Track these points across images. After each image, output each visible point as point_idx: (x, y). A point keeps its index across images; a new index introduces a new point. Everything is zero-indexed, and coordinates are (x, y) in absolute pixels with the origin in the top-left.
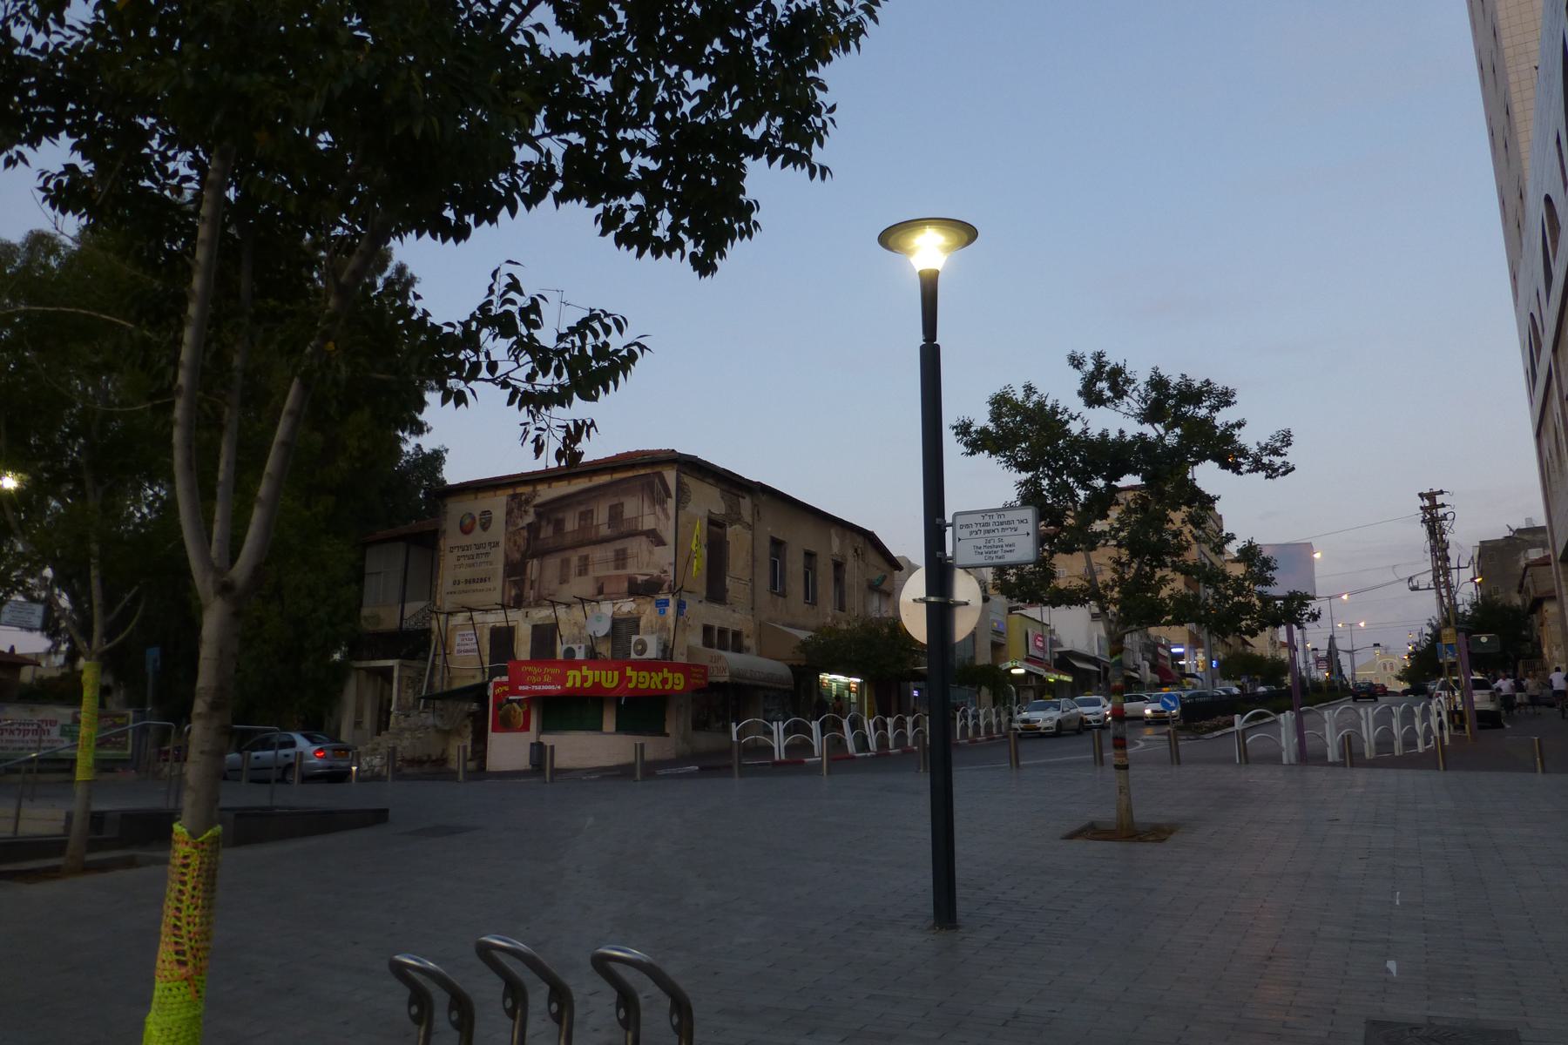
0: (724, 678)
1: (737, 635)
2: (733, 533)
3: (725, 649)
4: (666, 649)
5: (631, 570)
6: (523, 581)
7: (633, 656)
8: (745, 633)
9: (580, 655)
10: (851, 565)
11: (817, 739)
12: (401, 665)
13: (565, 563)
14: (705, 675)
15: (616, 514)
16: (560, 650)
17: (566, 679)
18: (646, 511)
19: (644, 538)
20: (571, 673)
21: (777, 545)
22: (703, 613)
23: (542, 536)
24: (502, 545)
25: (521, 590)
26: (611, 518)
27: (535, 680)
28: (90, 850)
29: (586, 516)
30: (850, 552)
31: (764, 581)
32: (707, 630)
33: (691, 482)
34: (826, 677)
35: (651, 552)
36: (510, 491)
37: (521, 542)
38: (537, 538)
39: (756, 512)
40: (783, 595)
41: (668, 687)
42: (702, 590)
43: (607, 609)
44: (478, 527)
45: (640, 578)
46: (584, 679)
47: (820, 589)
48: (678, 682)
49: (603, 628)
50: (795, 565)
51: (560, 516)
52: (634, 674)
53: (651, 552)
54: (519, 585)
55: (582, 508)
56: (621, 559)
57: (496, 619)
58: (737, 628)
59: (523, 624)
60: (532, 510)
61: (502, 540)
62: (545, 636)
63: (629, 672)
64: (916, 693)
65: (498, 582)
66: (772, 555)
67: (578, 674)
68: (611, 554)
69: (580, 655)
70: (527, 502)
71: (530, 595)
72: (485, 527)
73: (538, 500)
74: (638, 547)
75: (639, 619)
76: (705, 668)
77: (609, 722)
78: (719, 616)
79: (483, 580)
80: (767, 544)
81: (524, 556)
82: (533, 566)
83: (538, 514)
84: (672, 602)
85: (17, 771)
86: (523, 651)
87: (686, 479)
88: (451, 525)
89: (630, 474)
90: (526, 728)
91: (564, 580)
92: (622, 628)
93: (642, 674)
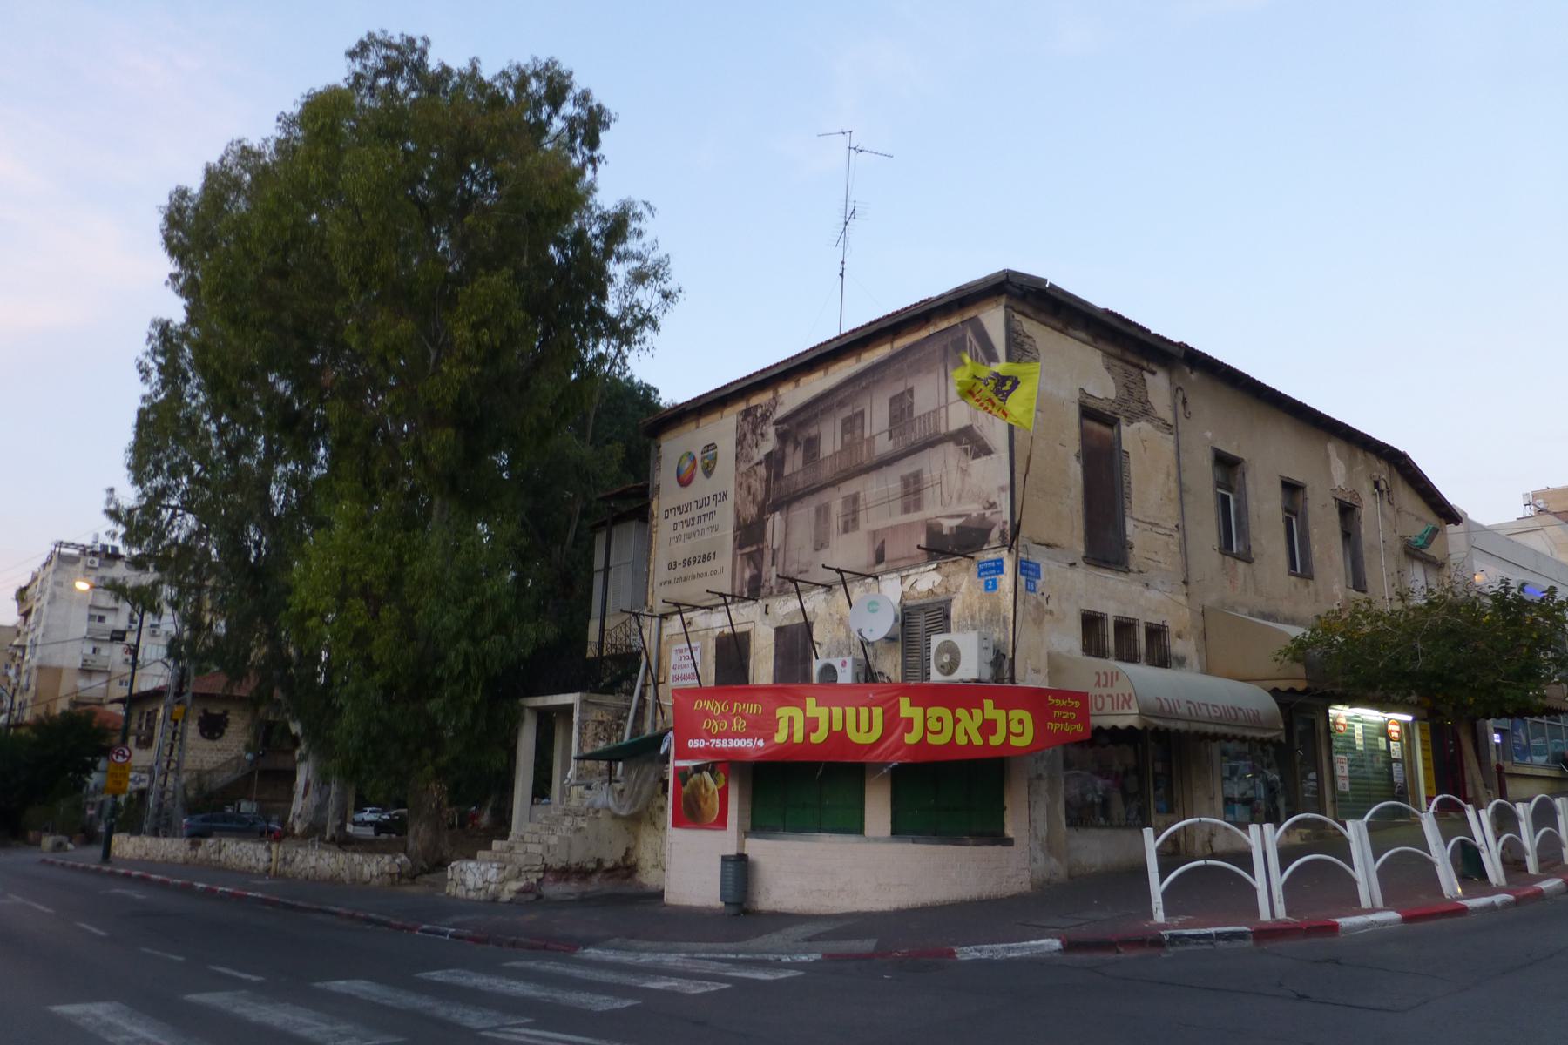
0: (1128, 718)
1: (1156, 633)
2: (1133, 435)
3: (1133, 659)
4: (1000, 660)
6: (761, 552)
7: (936, 677)
8: (1173, 627)
9: (845, 676)
10: (1371, 512)
11: (1364, 868)
12: (583, 701)
13: (823, 512)
14: (1083, 714)
15: (901, 410)
16: (816, 666)
17: (774, 726)
20: (783, 712)
21: (1227, 464)
22: (1078, 588)
23: (787, 471)
24: (731, 496)
25: (758, 567)
27: (716, 727)
29: (853, 423)
30: (1366, 489)
31: (1206, 532)
32: (1091, 622)
33: (1036, 331)
34: (1340, 713)
35: (964, 472)
36: (742, 406)
37: (758, 487)
38: (779, 476)
39: (1181, 401)
40: (1247, 559)
41: (996, 740)
42: (1074, 537)
43: (891, 589)
44: (699, 472)
45: (948, 525)
46: (811, 725)
47: (1316, 550)
48: (1018, 728)
49: (880, 625)
50: (1265, 504)
51: (813, 431)
52: (916, 714)
53: (964, 472)
54: (755, 559)
55: (847, 412)
56: (913, 491)
57: (717, 622)
58: (1156, 619)
59: (760, 624)
60: (770, 431)
61: (731, 489)
62: (795, 644)
63: (906, 708)
64: (1497, 738)
65: (725, 559)
66: (1218, 485)
67: (796, 712)
69: (845, 676)
70: (765, 418)
71: (771, 574)
72: (708, 472)
73: (780, 412)
74: (941, 465)
75: (949, 602)
76: (1083, 697)
77: (878, 810)
78: (1114, 596)
79: (706, 558)
80: (1207, 461)
81: (762, 510)
82: (775, 524)
83: (782, 437)
84: (1009, 566)
86: (762, 670)
87: (1029, 326)
88: (665, 476)
89: (923, 334)
90: (721, 822)
91: (821, 544)
92: (919, 623)
93: (935, 712)
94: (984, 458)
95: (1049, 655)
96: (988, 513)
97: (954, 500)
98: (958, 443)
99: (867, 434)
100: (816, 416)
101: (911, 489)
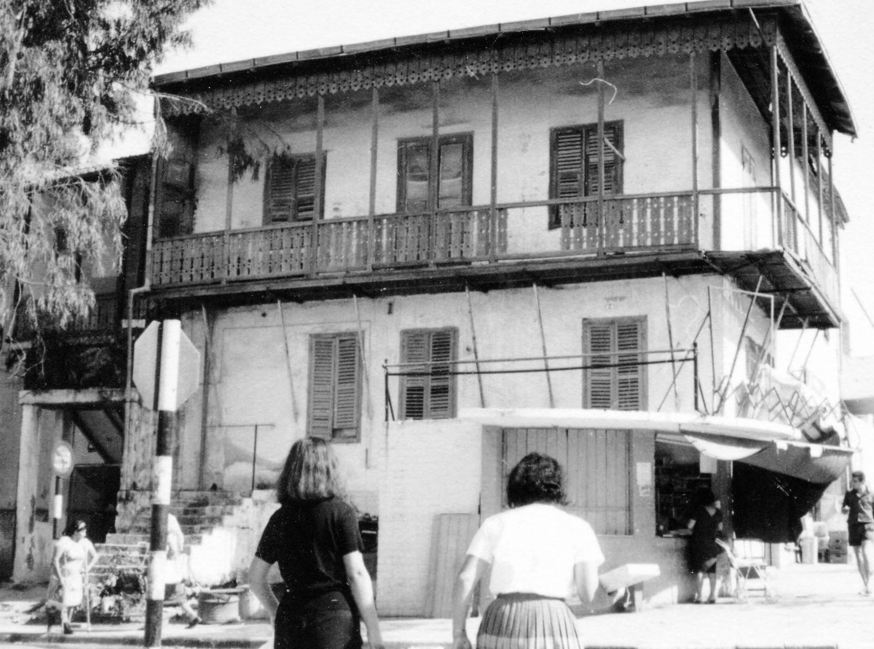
5: (666, 410)
6: (116, 413)
15: (584, 166)
18: (734, 171)
19: (725, 287)
26: (561, 182)
28: (753, 9)
35: (758, 352)
38: (173, 228)
53: (758, 352)
56: (615, 360)
60: (144, 104)
68: (567, 342)
73: (174, 61)
81: (114, 299)
82: (167, 359)
83: (187, 129)
85: (585, 181)
94: (810, 333)
95: (646, 317)
96: (816, 450)
97: (731, 404)
98: (746, 284)
99: (481, 197)
100: (310, 106)
101: (614, 354)
